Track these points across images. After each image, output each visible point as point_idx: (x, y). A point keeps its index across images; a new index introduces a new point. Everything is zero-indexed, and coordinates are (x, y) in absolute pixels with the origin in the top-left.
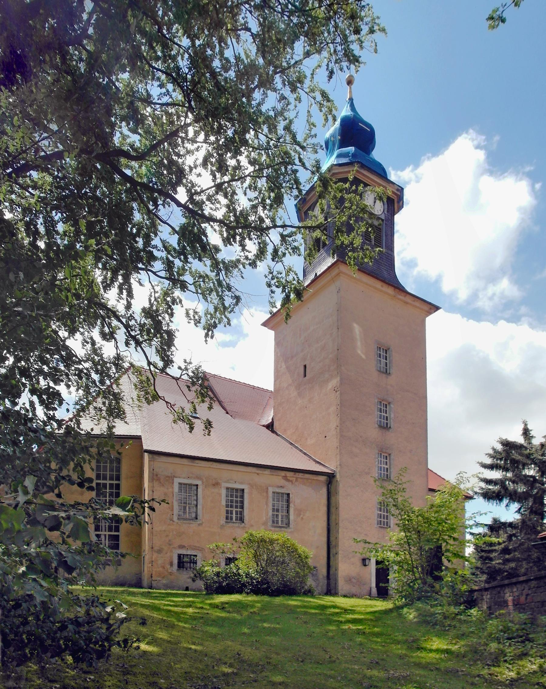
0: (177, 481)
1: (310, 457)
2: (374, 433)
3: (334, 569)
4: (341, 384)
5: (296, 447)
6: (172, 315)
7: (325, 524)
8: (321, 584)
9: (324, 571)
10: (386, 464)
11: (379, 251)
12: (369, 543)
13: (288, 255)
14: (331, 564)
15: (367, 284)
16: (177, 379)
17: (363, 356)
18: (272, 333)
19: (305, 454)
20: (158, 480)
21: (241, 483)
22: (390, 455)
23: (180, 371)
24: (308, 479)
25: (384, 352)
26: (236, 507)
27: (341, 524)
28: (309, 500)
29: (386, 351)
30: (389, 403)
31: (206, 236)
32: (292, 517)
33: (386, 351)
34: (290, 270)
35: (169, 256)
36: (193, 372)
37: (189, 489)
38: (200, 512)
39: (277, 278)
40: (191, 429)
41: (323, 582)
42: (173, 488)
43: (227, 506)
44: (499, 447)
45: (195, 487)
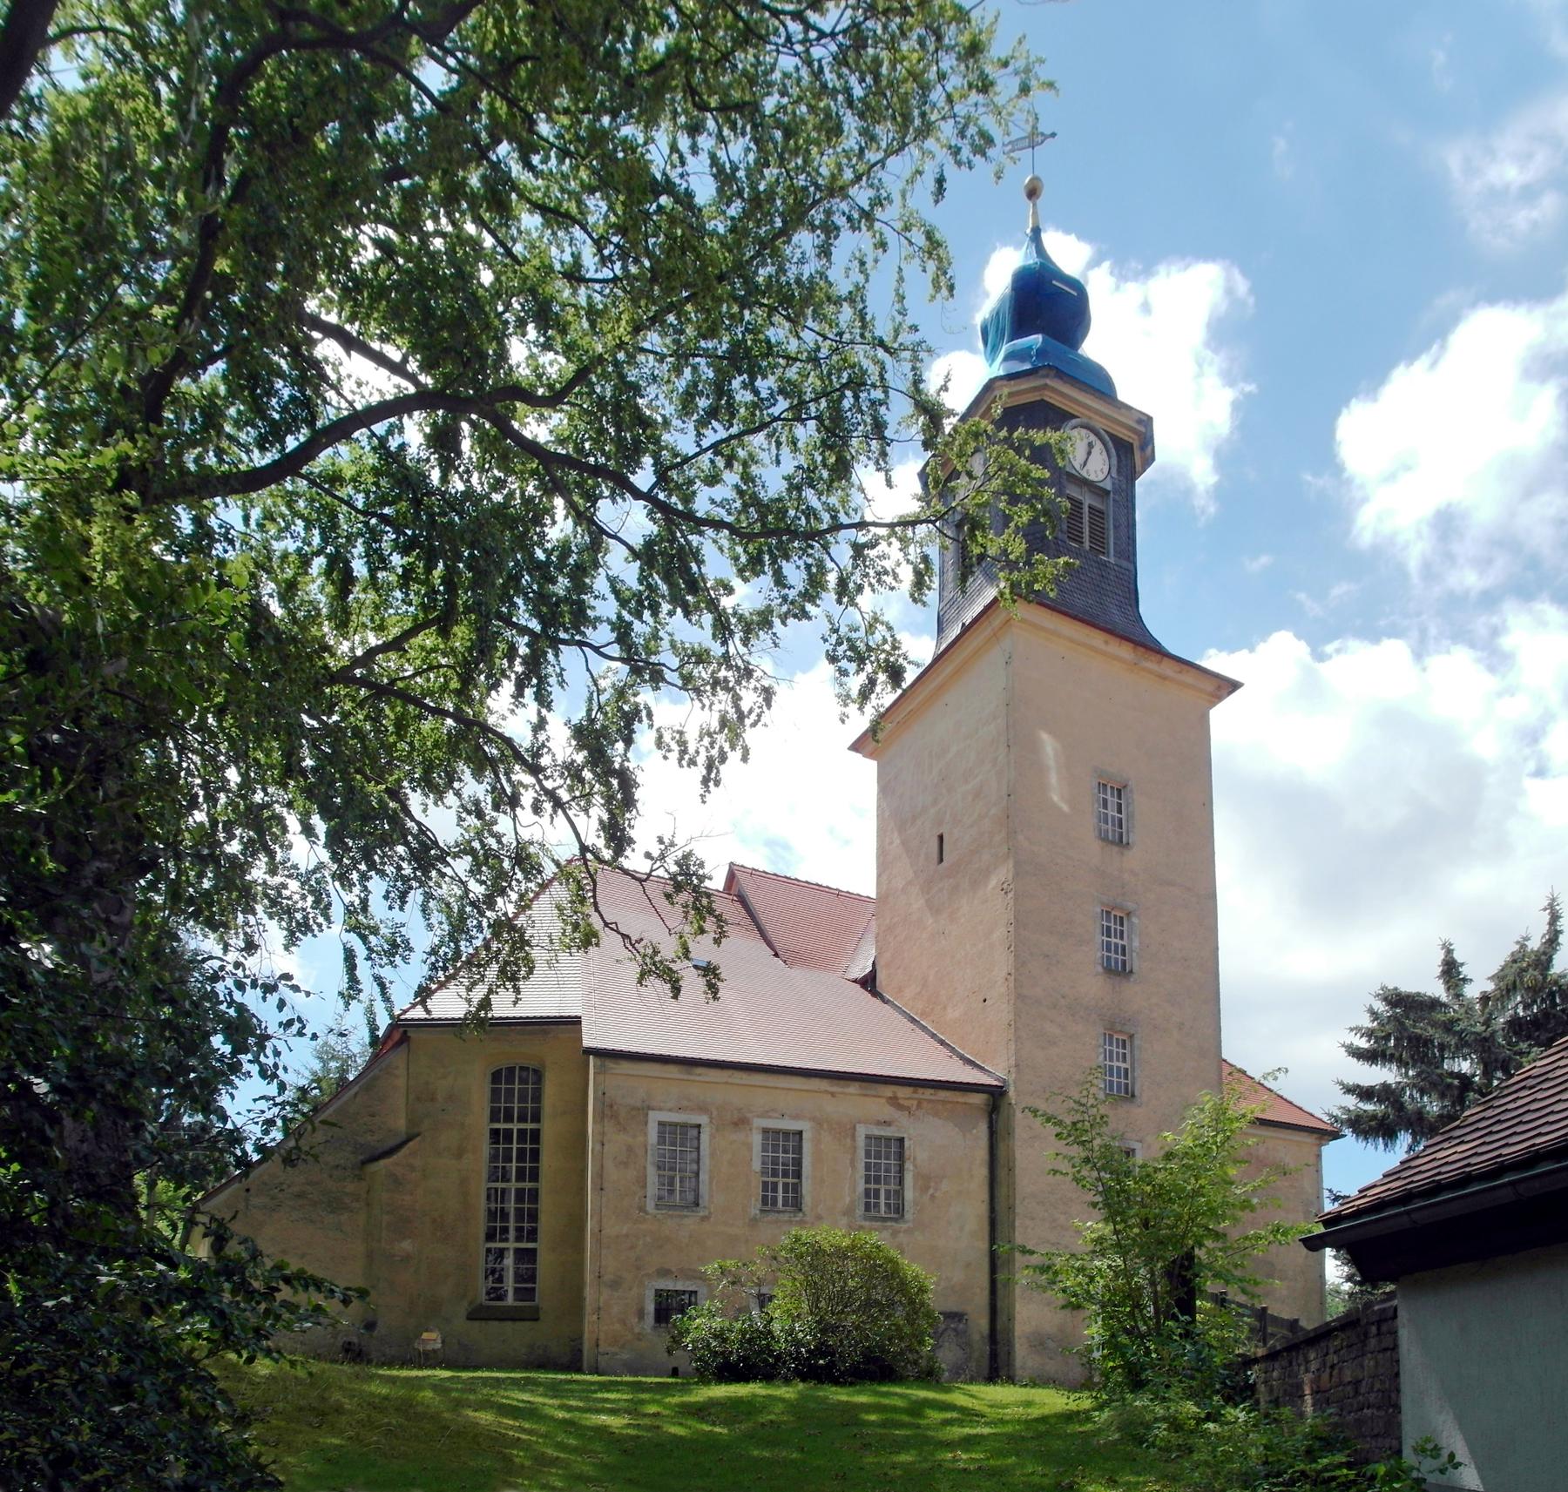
0: (654, 1117)
1: (953, 1050)
2: (1093, 986)
3: (1005, 1318)
4: (1017, 875)
5: (924, 1028)
6: (629, 742)
7: (983, 1209)
8: (976, 1354)
9: (983, 1323)
10: (1124, 1061)
11: (1066, 563)
12: (1032, 1253)
13: (867, 589)
14: (999, 1304)
15: (1071, 640)
16: (641, 880)
17: (1065, 808)
18: (871, 766)
19: (942, 1043)
20: (614, 1116)
21: (796, 1117)
22: (1131, 1037)
23: (650, 862)
24: (944, 1102)
25: (1114, 792)
26: (785, 1174)
27: (1019, 1209)
28: (945, 1149)
29: (1119, 791)
30: (1128, 914)
31: (700, 563)
32: (909, 1195)
33: (1119, 791)
34: (876, 620)
35: (624, 613)
36: (677, 863)
37: (679, 1136)
38: (704, 1189)
39: (849, 640)
40: (676, 991)
41: (981, 1348)
42: (646, 1134)
43: (764, 1173)
44: (1380, 1007)
45: (695, 1132)
